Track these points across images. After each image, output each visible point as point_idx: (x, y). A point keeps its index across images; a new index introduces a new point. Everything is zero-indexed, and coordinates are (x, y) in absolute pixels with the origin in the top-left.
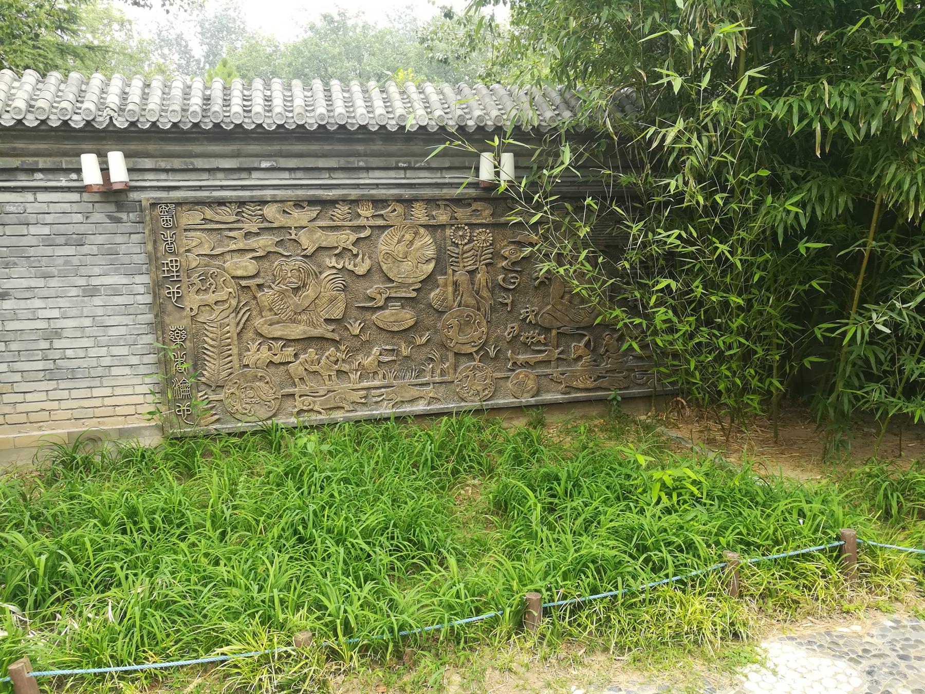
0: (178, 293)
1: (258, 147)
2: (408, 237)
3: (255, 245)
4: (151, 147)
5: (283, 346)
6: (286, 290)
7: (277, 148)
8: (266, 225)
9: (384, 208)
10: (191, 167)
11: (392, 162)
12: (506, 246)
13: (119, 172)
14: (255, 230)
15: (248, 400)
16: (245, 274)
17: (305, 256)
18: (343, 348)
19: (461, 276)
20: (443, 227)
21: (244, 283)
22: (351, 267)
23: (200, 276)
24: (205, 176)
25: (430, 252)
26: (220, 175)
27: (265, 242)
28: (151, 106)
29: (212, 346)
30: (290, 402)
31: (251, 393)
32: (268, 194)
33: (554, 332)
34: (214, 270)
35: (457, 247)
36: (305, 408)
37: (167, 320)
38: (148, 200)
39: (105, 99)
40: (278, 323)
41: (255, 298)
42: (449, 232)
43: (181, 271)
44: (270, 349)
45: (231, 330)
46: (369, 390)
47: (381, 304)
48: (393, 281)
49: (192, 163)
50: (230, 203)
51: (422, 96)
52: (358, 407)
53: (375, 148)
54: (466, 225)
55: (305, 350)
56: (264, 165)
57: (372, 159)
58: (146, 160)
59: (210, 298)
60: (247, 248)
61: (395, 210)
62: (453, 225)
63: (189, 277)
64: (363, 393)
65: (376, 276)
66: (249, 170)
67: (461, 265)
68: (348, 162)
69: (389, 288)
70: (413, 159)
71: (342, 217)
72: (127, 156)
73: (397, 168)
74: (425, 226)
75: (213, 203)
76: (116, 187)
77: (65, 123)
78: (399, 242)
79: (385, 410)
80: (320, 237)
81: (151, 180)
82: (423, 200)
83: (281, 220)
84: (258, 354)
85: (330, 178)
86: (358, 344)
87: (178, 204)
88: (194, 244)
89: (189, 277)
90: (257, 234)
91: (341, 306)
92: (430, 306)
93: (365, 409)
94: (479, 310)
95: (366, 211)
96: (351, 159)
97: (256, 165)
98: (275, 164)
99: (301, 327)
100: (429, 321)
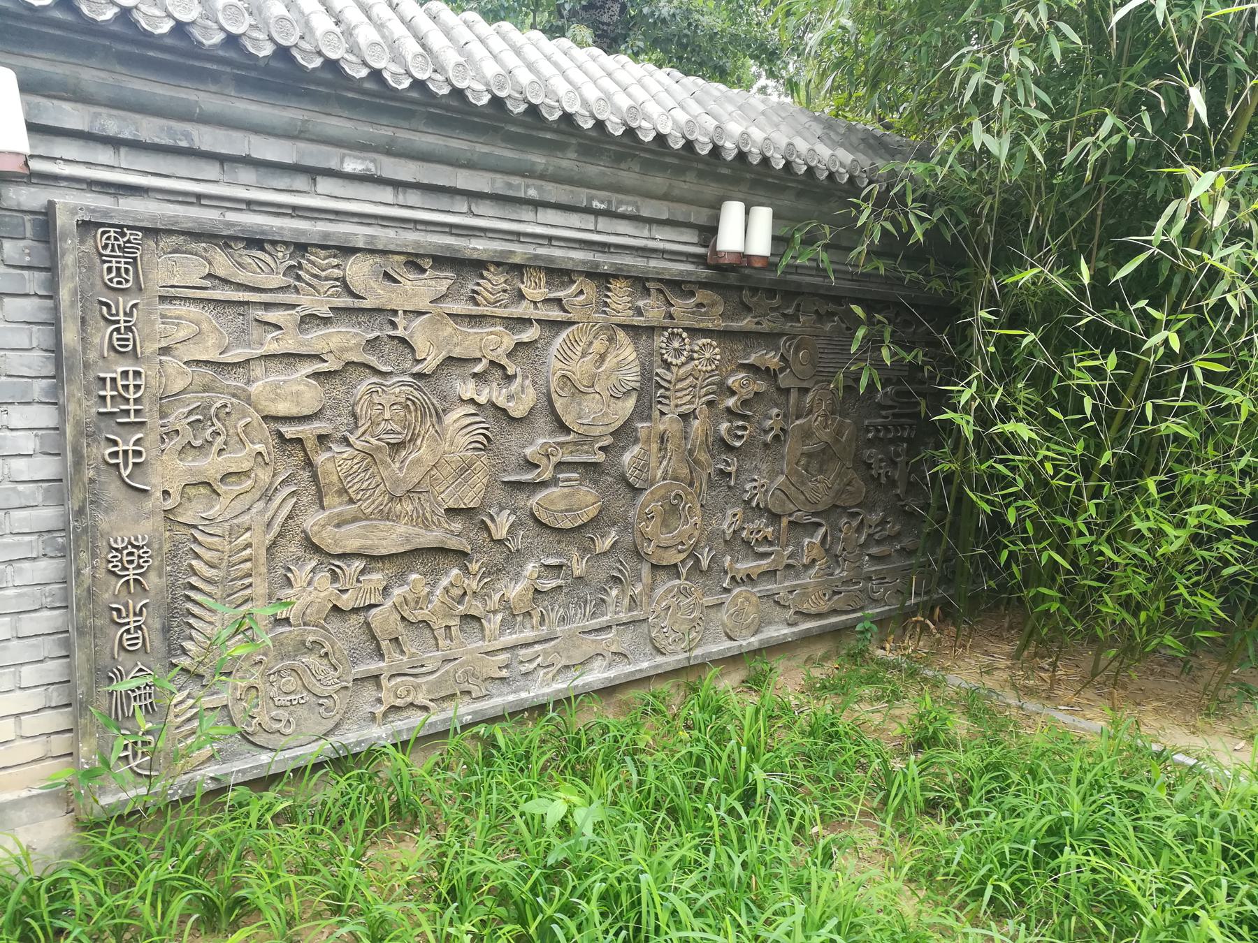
0: (138, 453)
1: (348, 125)
2: (598, 346)
3: (319, 347)
4: (90, 76)
5: (362, 572)
6: (378, 449)
7: (387, 132)
8: (345, 301)
9: (564, 285)
10: (184, 144)
11: (581, 196)
12: (733, 372)
14: (324, 311)
15: (284, 700)
16: (294, 411)
17: (419, 376)
18: (474, 567)
19: (668, 424)
20: (651, 330)
21: (289, 431)
22: (501, 401)
23: (190, 413)
24: (212, 171)
25: (632, 377)
26: (247, 175)
27: (341, 340)
29: (208, 581)
30: (369, 692)
31: (290, 682)
32: (359, 233)
33: (785, 521)
34: (226, 399)
35: (669, 369)
36: (399, 702)
37: (104, 521)
38: (73, 211)
40: (355, 520)
41: (309, 464)
42: (659, 341)
43: (146, 401)
44: (335, 577)
45: (254, 541)
46: (548, 651)
47: (547, 476)
48: (567, 430)
49: (187, 136)
50: (274, 243)
52: (494, 688)
53: (565, 164)
54: (685, 329)
55: (401, 578)
56: (351, 166)
57: (549, 186)
58: (67, 106)
59: (211, 465)
60: (304, 351)
61: (581, 292)
62: (665, 329)
63: (163, 415)
64: (503, 657)
65: (542, 422)
66: (313, 173)
67: (673, 403)
68: (510, 185)
69: (561, 445)
70: (615, 197)
71: (492, 298)
73: (588, 210)
74: (624, 327)
75: (236, 239)
78: (584, 354)
79: (542, 689)
80: (451, 336)
81: (69, 159)
82: (627, 277)
83: (378, 295)
84: (312, 589)
85: (471, 213)
86: (500, 558)
87: (152, 232)
88: (182, 334)
89: (163, 415)
90: (326, 321)
91: (480, 480)
92: (623, 479)
93: (505, 689)
94: (691, 484)
95: (535, 289)
96: (516, 180)
97: (333, 164)
98: (372, 166)
99: (402, 529)
100: (618, 507)
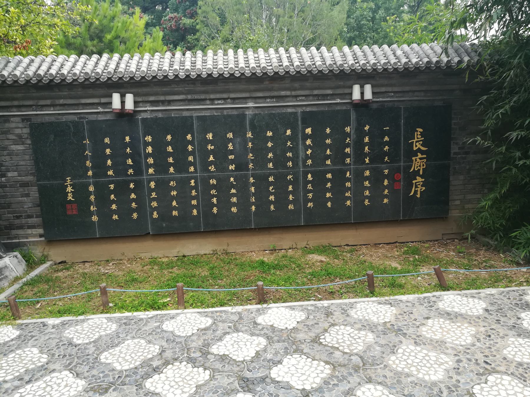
13: (129, 105)
28: (120, 70)
39: (130, 66)
51: (299, 55)
72: (135, 96)
76: (354, 102)
77: (177, 76)
